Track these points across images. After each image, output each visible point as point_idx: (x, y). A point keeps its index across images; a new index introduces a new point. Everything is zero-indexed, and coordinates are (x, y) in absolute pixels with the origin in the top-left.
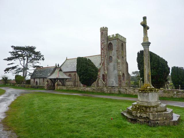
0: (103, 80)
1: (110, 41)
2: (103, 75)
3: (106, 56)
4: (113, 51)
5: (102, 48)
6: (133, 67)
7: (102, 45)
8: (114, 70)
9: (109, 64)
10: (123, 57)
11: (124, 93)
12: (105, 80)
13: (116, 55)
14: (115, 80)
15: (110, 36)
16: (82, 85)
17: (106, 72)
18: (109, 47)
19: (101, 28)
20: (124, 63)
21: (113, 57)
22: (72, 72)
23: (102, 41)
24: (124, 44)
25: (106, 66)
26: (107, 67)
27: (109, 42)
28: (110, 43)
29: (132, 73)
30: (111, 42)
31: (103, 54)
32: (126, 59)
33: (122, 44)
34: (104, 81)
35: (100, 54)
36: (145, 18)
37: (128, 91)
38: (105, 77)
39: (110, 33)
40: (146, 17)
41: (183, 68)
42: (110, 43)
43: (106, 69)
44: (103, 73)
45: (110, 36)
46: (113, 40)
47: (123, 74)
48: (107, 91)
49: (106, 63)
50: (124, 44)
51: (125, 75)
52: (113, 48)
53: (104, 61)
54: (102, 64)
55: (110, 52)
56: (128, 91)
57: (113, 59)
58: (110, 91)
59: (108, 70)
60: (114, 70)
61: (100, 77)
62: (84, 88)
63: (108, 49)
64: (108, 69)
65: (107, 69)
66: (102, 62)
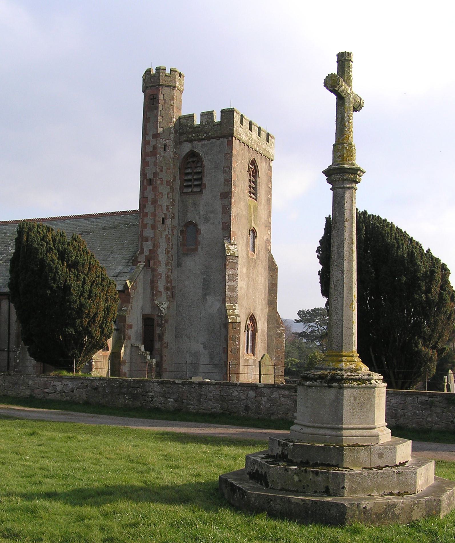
0: (144, 343)
1: (191, 141)
2: (149, 322)
3: (168, 222)
4: (206, 192)
5: (150, 176)
6: (301, 292)
7: (148, 159)
8: (204, 296)
9: (179, 265)
10: (253, 232)
11: (247, 408)
12: (157, 345)
13: (220, 215)
14: (205, 347)
15: (191, 116)
16: (31, 362)
17: (164, 306)
18: (183, 174)
19: (148, 71)
20: (255, 261)
21: (203, 228)
22: (270, 212)
23: (149, 137)
24: (264, 164)
25: (162, 269)
26: (169, 280)
27: (187, 148)
28: (193, 154)
29: (298, 318)
30: (198, 148)
31: (149, 209)
32: (268, 241)
33: (253, 163)
34: (149, 348)
35: (136, 207)
36: (344, 60)
37: (264, 399)
38: (158, 330)
39: (193, 102)
40: (349, 54)
41: (319, 272)
42: (193, 154)
43: (161, 288)
44: (148, 311)
45: (191, 116)
46: (208, 138)
47: (252, 318)
48: (162, 399)
49: (162, 257)
50: (262, 167)
51: (262, 325)
52: (205, 181)
53: (155, 246)
54: (142, 259)
55: (190, 200)
56: (264, 399)
57: (200, 238)
58: (176, 401)
59: (173, 296)
60: (204, 296)
61: (130, 327)
62: (43, 379)
63: (178, 181)
64: (171, 290)
65: (167, 289)
66: (146, 252)
